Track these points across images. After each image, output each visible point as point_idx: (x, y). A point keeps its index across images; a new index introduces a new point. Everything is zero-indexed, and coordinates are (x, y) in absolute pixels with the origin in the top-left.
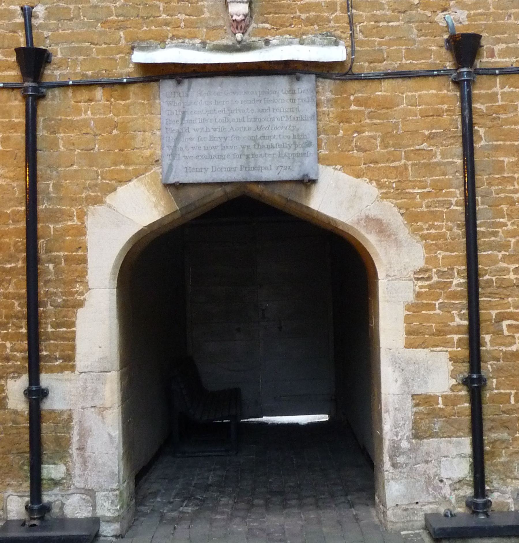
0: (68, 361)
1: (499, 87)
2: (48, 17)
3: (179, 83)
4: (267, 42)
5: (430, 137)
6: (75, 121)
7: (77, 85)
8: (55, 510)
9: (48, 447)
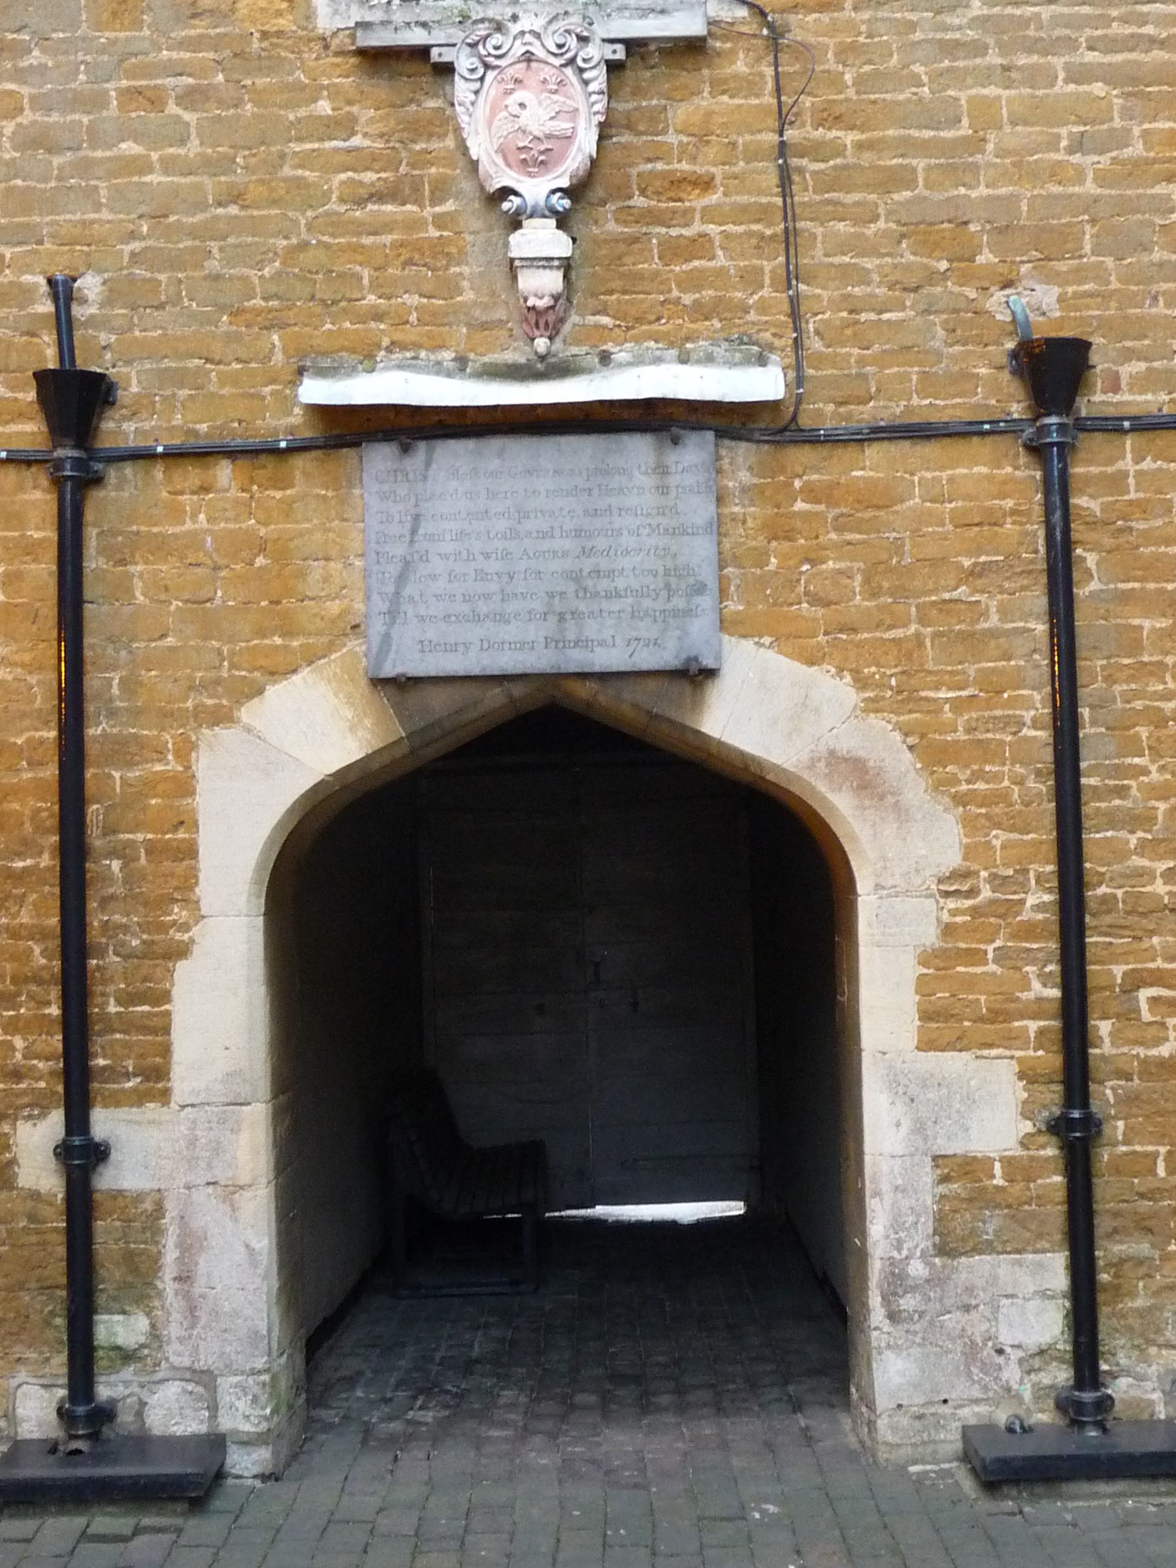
0: (155, 1079)
1: (1130, 460)
2: (108, 302)
3: (406, 449)
4: (605, 358)
5: (976, 573)
6: (171, 538)
7: (175, 456)
8: (125, 1418)
9: (110, 1275)
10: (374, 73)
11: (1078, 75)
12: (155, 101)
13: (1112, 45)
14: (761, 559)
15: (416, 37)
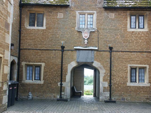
0: (65, 81)
1: (114, 53)
2: (65, 43)
3: (79, 51)
4: (89, 47)
5: (107, 58)
6: (67, 54)
7: (68, 50)
8: (63, 98)
9: (62, 90)
10: (78, 32)
11: (113, 34)
12: (67, 33)
13: (115, 33)
14: (96, 57)
15: (80, 31)
